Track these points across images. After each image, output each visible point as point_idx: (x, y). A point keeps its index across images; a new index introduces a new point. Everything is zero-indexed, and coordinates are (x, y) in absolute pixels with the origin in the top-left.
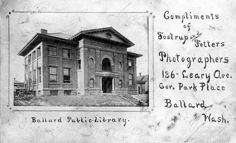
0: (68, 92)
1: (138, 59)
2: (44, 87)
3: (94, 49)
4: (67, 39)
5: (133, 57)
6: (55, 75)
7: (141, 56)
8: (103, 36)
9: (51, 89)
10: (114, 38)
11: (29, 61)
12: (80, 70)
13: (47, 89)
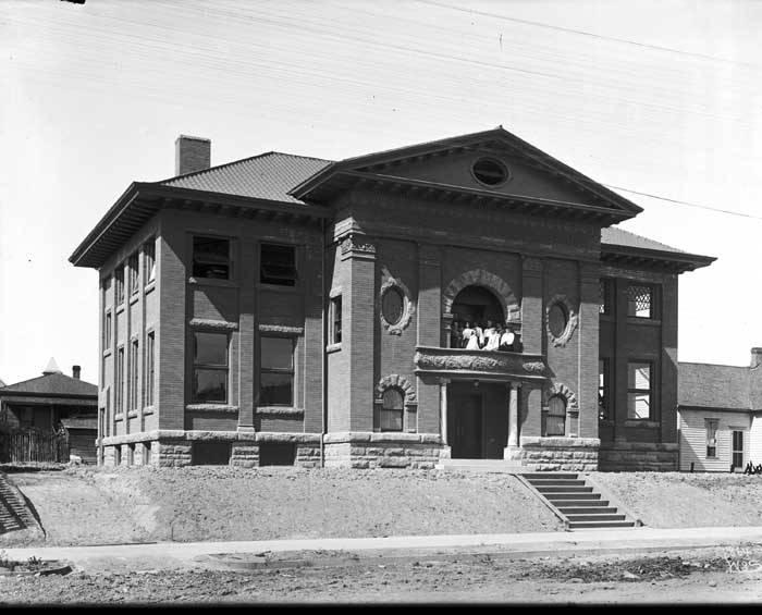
0: (275, 454)
1: (686, 281)
2: (164, 423)
3: (413, 242)
4: (492, 128)
5: (664, 268)
6: (330, 352)
7: (715, 259)
8: (462, 180)
9: (195, 434)
10: (516, 187)
11: (118, 299)
12: (338, 345)
13: (180, 432)
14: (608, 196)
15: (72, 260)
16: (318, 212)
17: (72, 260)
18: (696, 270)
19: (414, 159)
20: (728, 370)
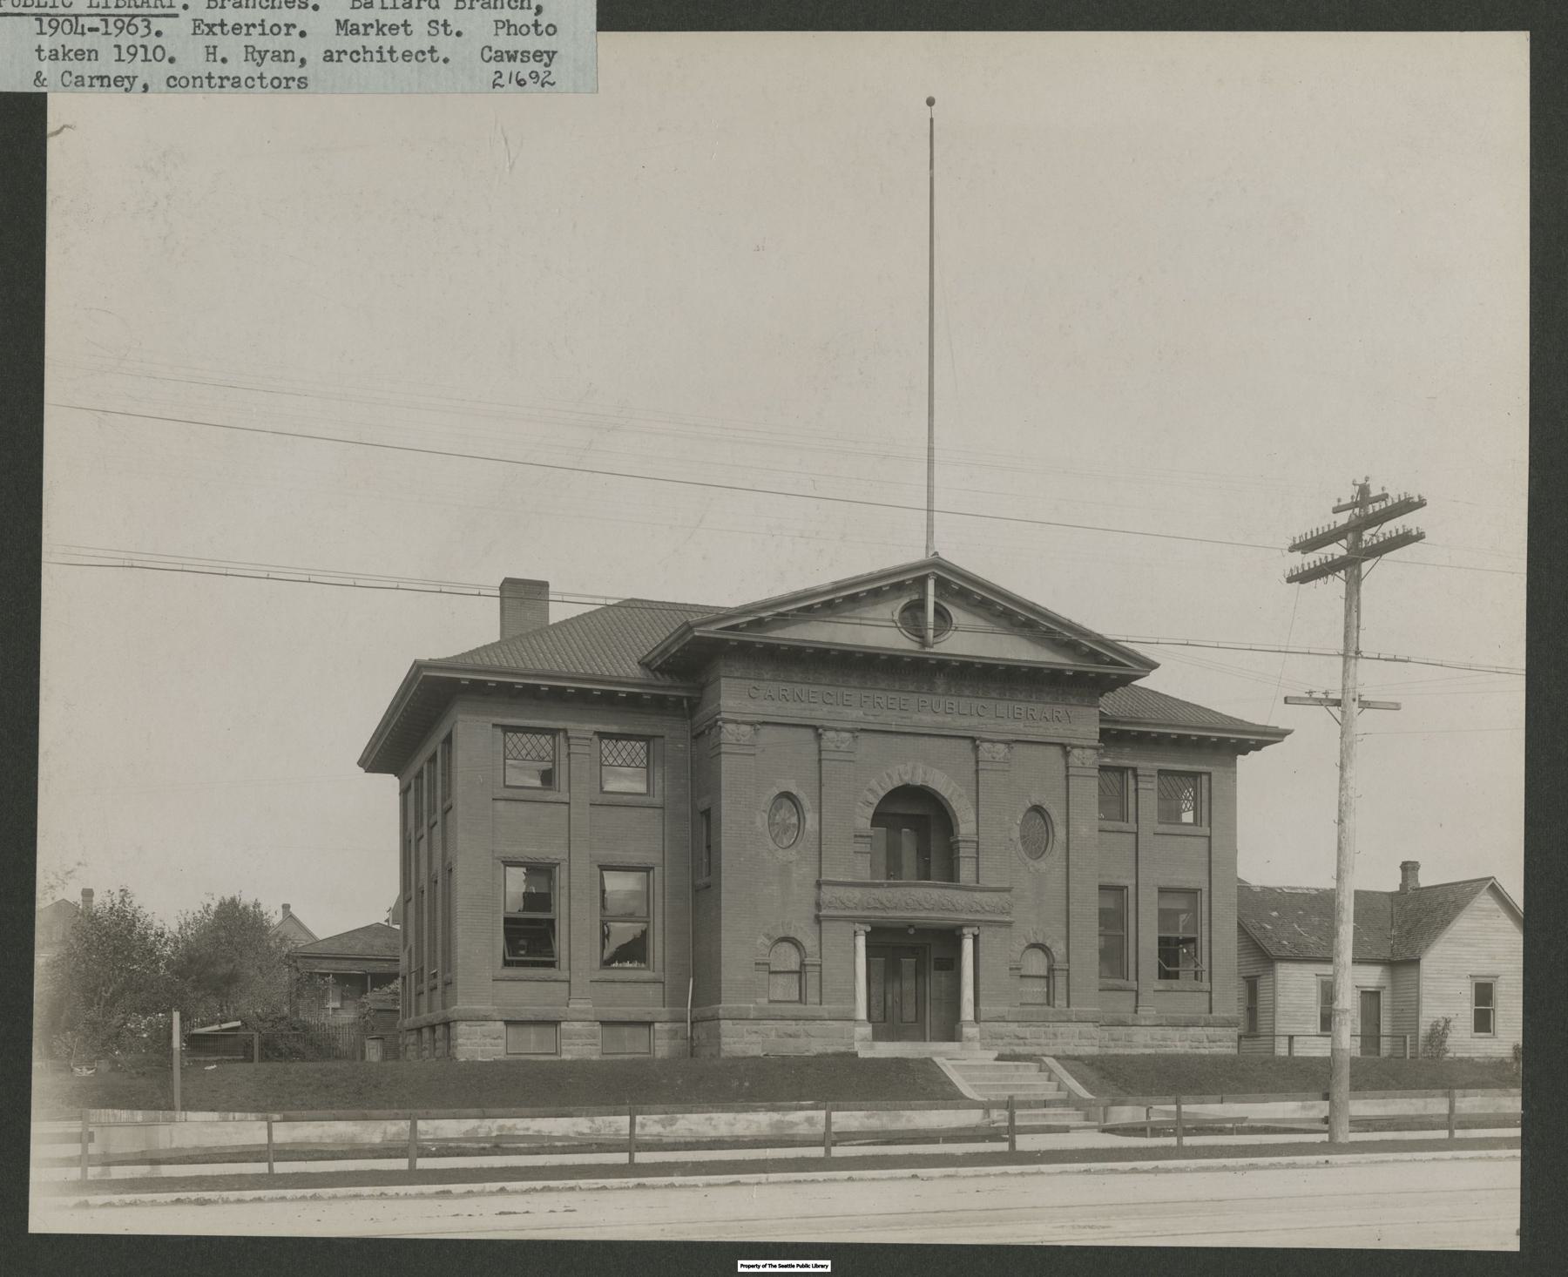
14: (378, 740)
15: (361, 763)
16: (675, 690)
17: (361, 763)
18: (1264, 749)
19: (809, 609)
20: (237, 1187)
